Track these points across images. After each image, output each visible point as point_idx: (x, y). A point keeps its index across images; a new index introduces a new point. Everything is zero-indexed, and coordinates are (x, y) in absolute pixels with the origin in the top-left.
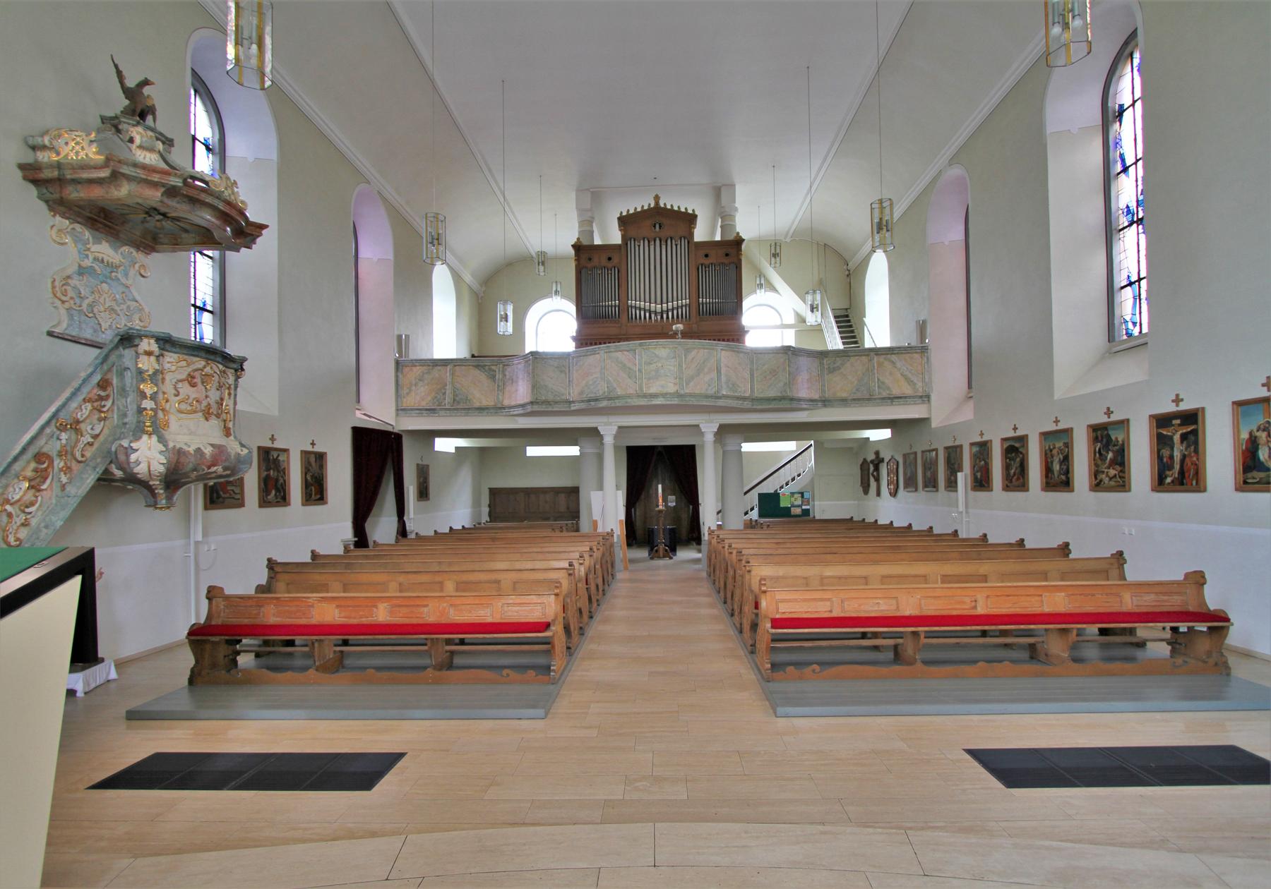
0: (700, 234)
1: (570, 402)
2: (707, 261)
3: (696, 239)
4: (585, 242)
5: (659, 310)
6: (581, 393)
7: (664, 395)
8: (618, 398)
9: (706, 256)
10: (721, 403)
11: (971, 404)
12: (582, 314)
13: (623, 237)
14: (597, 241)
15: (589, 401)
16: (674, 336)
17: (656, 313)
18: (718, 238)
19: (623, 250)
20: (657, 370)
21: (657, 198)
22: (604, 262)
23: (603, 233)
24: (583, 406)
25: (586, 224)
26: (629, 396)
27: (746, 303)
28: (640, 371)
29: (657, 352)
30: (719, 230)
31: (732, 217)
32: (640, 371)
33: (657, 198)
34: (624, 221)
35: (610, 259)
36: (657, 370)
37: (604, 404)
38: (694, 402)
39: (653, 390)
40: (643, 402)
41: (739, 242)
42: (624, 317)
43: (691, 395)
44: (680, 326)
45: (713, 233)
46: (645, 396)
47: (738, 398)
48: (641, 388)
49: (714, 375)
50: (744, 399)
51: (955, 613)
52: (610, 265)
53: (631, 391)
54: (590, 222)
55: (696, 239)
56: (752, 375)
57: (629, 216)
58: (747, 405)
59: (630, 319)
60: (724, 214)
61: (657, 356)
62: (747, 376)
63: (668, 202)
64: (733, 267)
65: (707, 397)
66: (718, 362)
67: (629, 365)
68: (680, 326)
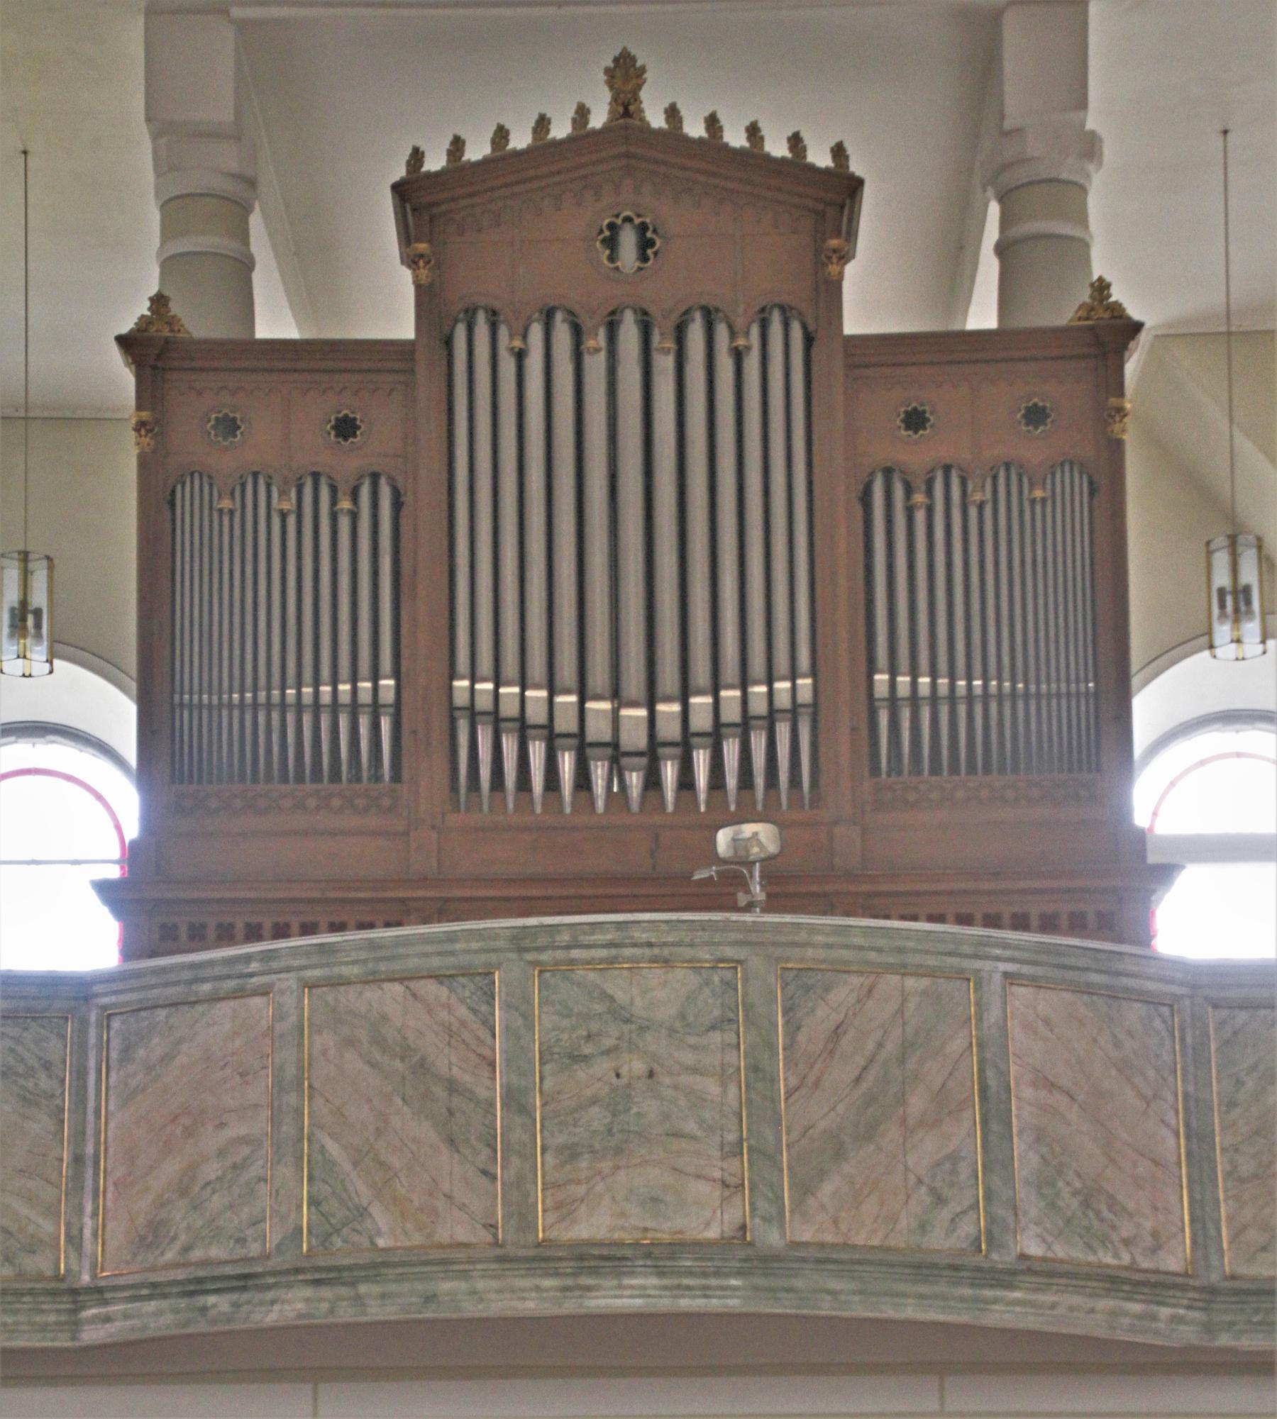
0: (872, 298)
1: (77, 1296)
2: (917, 454)
3: (852, 326)
4: (200, 322)
5: (634, 737)
6: (152, 1234)
7: (662, 1256)
8: (379, 1266)
9: (915, 420)
10: (1008, 1310)
11: (797, 1215)
12: (167, 750)
13: (426, 299)
14: (275, 322)
15: (196, 1287)
16: (724, 890)
17: (616, 754)
18: (982, 316)
19: (427, 384)
20: (618, 1099)
21: (625, 76)
22: (312, 444)
23: (314, 269)
24: (158, 1317)
25: (211, 221)
26: (449, 1260)
27: (1149, 708)
28: (516, 1101)
29: (618, 986)
30: (988, 269)
31: (1069, 197)
32: (516, 1101)
33: (625, 76)
34: (423, 203)
35: (346, 428)
36: (618, 1099)
37: (291, 1305)
38: (841, 1298)
39: (592, 1226)
40: (532, 1297)
41: (1110, 332)
42: (428, 775)
43: (824, 1258)
44: (761, 835)
45: (954, 279)
46: (543, 1258)
47: (897, 1295)
48: (523, 1216)
49: (965, 1133)
50: (1157, 1286)
51: (396, 214)
52: (347, 462)
53: (455, 1228)
54: (234, 210)
55: (852, 326)
56: (1199, 1138)
57: (458, 169)
58: (1176, 1325)
59: (461, 786)
60: (1021, 184)
61: (620, 1014)
62: (1172, 1146)
63: (680, 99)
64: (1073, 486)
65: (924, 1269)
66: (991, 1053)
67: (448, 1061)
68: (761, 835)
